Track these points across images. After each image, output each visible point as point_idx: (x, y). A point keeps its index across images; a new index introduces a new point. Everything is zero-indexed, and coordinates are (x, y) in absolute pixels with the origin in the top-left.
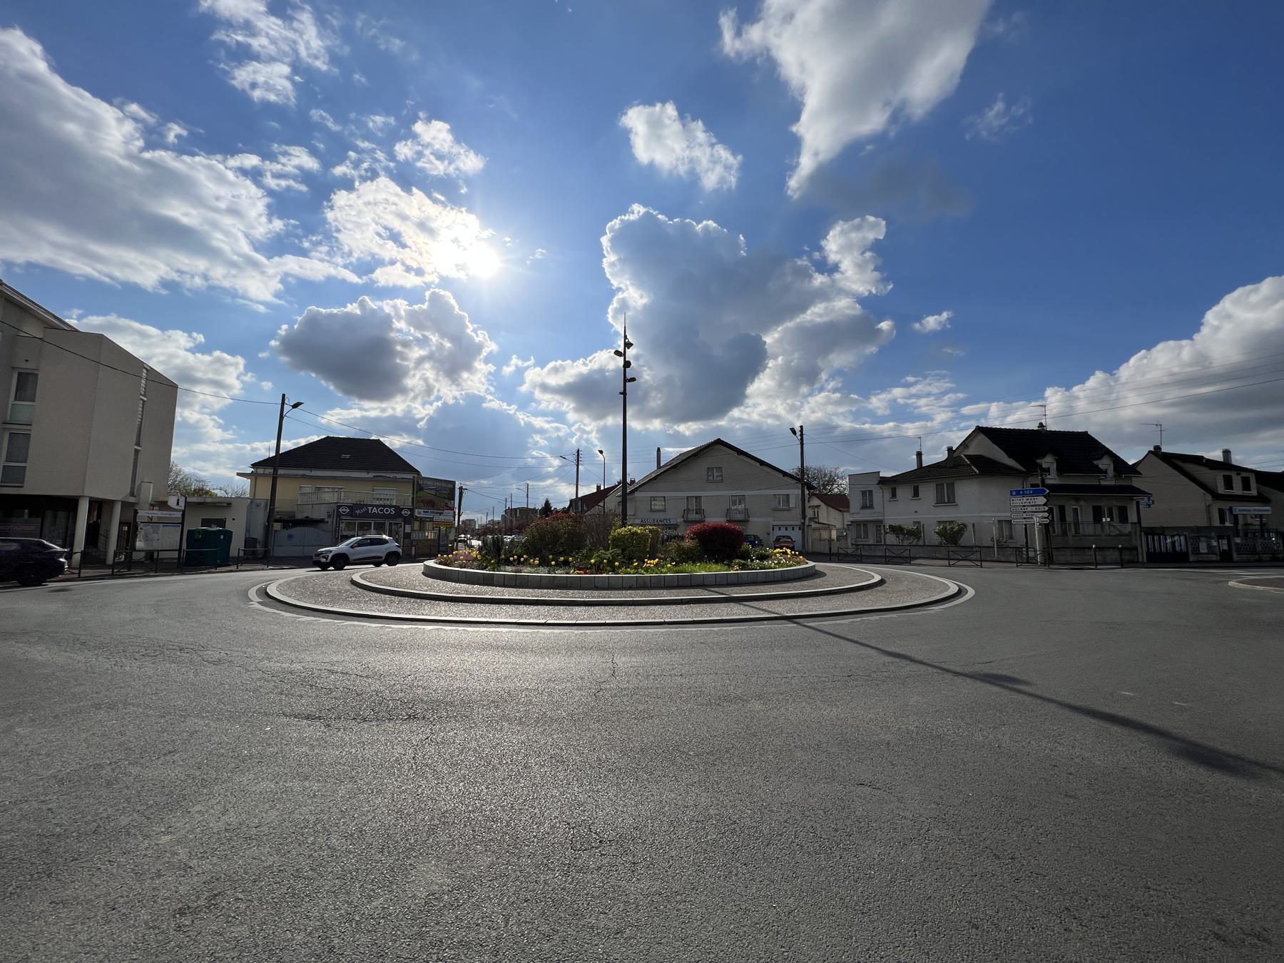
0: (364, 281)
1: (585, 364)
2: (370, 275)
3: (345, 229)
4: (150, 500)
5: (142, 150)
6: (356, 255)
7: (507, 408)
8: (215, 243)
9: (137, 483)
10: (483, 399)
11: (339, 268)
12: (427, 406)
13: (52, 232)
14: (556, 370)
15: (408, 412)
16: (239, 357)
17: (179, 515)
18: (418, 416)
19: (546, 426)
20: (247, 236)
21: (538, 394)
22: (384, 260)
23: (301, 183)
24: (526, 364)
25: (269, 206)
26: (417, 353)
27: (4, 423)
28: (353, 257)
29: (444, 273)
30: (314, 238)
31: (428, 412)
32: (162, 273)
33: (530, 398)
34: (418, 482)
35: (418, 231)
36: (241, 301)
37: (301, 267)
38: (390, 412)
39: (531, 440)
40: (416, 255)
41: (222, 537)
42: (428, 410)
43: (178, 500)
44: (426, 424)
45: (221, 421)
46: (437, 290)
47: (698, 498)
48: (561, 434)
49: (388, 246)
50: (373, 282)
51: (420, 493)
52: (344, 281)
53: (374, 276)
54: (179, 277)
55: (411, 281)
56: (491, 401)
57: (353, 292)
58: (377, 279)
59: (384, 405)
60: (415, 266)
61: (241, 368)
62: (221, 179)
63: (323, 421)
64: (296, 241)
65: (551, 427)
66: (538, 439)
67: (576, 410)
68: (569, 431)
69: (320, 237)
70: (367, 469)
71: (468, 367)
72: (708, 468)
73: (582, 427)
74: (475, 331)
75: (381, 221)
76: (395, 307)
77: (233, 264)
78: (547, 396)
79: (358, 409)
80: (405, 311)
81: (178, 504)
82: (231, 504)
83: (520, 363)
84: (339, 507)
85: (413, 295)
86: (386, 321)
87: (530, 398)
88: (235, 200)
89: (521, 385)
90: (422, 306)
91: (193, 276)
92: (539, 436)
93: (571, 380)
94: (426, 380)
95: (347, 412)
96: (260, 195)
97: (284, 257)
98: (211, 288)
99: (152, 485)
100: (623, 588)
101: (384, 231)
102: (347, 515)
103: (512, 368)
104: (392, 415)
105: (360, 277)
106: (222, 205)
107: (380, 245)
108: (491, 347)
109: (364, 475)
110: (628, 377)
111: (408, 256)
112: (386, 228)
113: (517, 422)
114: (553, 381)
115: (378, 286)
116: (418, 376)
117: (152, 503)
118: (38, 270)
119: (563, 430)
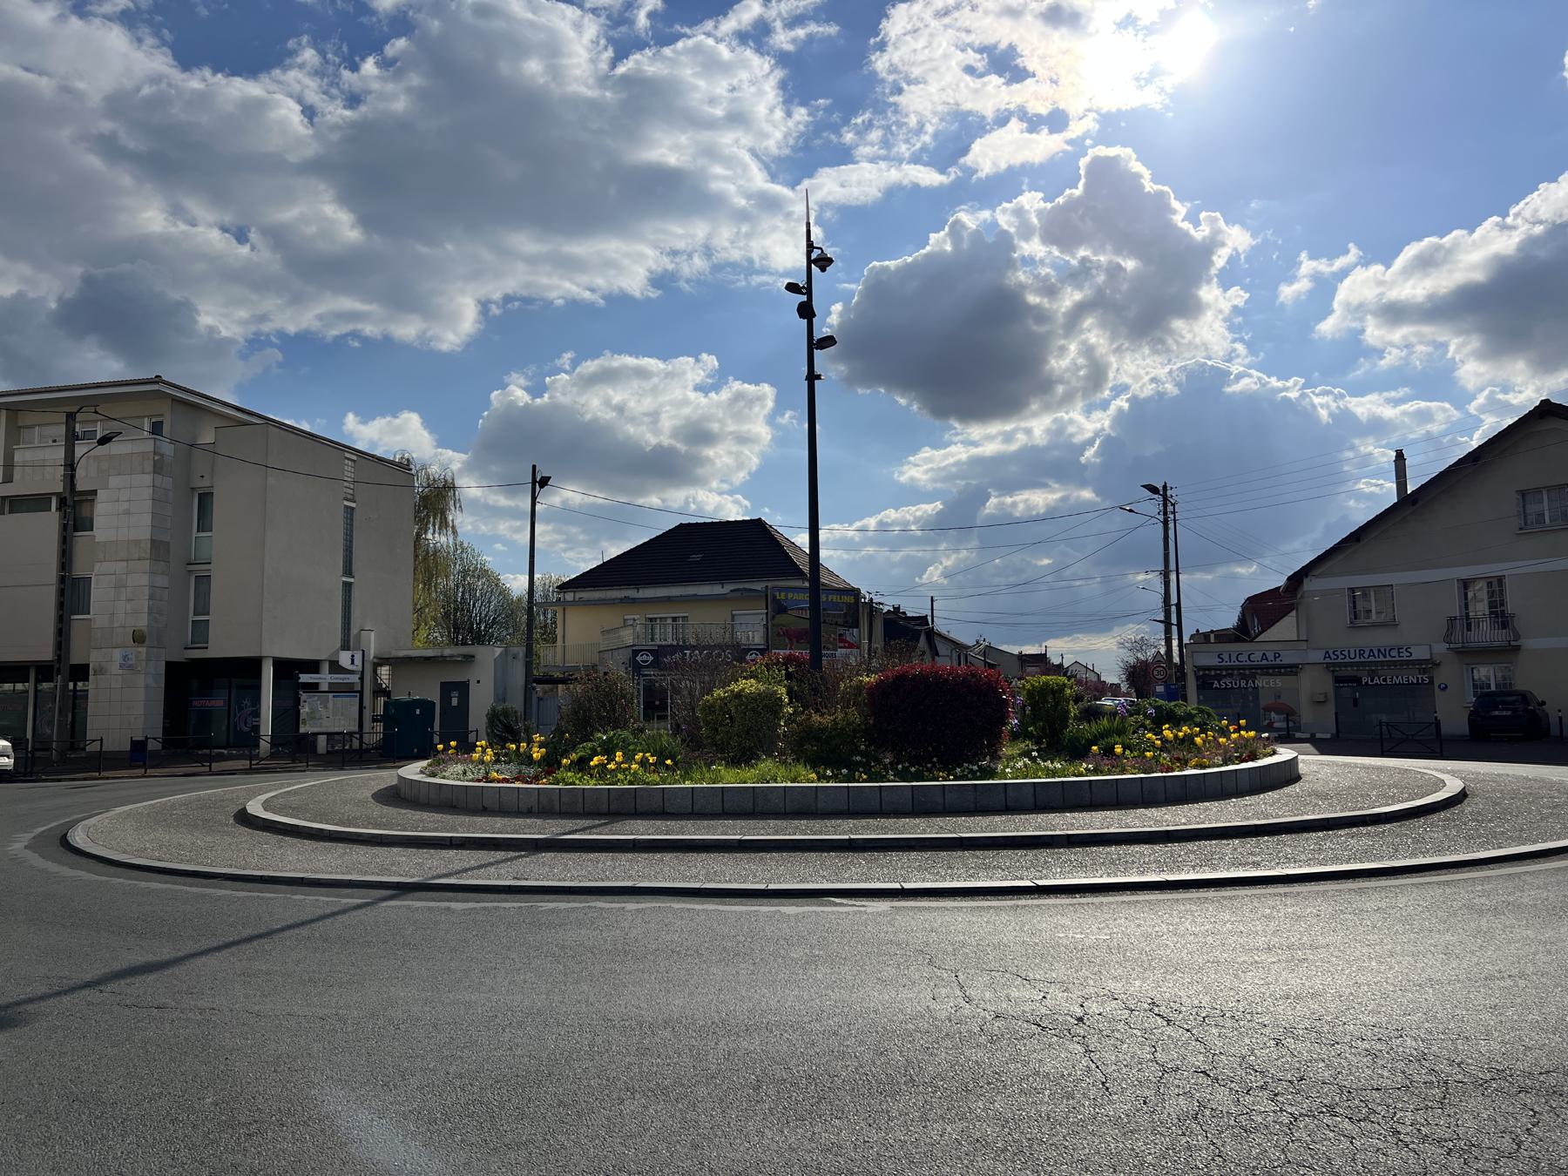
0: (953, 177)
1: (1504, 227)
2: (962, 161)
3: (909, 83)
4: (372, 657)
5: (614, 63)
6: (930, 129)
7: (1280, 384)
8: (715, 186)
9: (354, 631)
10: (1222, 376)
11: (905, 167)
12: (1097, 414)
13: (525, 242)
14: (1425, 263)
15: (1058, 431)
16: (766, 385)
17: (355, 679)
18: (1078, 439)
19: (1389, 413)
20: (754, 153)
21: (1374, 332)
22: (983, 118)
23: (827, 21)
24: (1339, 263)
25: (783, 85)
26: (1071, 297)
27: (188, 564)
28: (926, 133)
29: (1109, 104)
30: (859, 120)
31: (1098, 426)
32: (651, 264)
33: (1353, 348)
34: (774, 597)
35: (1048, 30)
36: (757, 280)
37: (843, 186)
38: (1021, 438)
39: (1349, 454)
40: (1046, 89)
41: (418, 712)
42: (1099, 420)
43: (353, 656)
44: (1097, 454)
45: (746, 503)
46: (1103, 151)
47: (1496, 586)
48: (1434, 428)
49: (990, 88)
50: (970, 171)
51: (781, 619)
52: (916, 187)
53: (968, 160)
54: (672, 262)
55: (1044, 146)
56: (1240, 377)
57: (933, 206)
58: (977, 164)
59: (1009, 427)
60: (1043, 109)
61: (770, 404)
62: (712, 65)
63: (903, 479)
64: (833, 137)
65: (1404, 413)
66: (1371, 448)
67: (1485, 355)
68: (1456, 414)
69: (867, 116)
70: (720, 578)
71: (1189, 307)
72: (1523, 494)
73: (1501, 396)
74: (1193, 218)
75: (969, 39)
76: (1019, 212)
77: (742, 216)
78: (1399, 334)
79: (962, 442)
80: (1040, 213)
81: (353, 663)
82: (473, 657)
83: (1323, 266)
84: (636, 653)
85: (1047, 176)
86: (998, 249)
87: (1353, 348)
88: (735, 94)
89: (1323, 317)
90: (1074, 191)
91: (690, 256)
92: (1370, 440)
93: (1479, 276)
94: (1088, 351)
95: (942, 452)
96: (767, 67)
97: (817, 175)
98: (717, 268)
99: (373, 633)
100: (485, 811)
101: (978, 56)
102: (651, 666)
103: (1303, 285)
104: (1026, 445)
105: (942, 171)
106: (719, 112)
107: (976, 91)
108: (1237, 239)
109: (717, 589)
110: (817, 336)
111: (1032, 96)
112: (981, 50)
113: (1309, 415)
114: (1416, 290)
115: (980, 179)
116: (1073, 347)
117: (375, 660)
118: (516, 304)
119: (1440, 417)
